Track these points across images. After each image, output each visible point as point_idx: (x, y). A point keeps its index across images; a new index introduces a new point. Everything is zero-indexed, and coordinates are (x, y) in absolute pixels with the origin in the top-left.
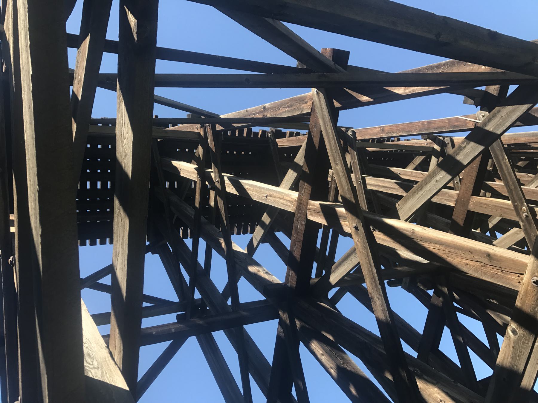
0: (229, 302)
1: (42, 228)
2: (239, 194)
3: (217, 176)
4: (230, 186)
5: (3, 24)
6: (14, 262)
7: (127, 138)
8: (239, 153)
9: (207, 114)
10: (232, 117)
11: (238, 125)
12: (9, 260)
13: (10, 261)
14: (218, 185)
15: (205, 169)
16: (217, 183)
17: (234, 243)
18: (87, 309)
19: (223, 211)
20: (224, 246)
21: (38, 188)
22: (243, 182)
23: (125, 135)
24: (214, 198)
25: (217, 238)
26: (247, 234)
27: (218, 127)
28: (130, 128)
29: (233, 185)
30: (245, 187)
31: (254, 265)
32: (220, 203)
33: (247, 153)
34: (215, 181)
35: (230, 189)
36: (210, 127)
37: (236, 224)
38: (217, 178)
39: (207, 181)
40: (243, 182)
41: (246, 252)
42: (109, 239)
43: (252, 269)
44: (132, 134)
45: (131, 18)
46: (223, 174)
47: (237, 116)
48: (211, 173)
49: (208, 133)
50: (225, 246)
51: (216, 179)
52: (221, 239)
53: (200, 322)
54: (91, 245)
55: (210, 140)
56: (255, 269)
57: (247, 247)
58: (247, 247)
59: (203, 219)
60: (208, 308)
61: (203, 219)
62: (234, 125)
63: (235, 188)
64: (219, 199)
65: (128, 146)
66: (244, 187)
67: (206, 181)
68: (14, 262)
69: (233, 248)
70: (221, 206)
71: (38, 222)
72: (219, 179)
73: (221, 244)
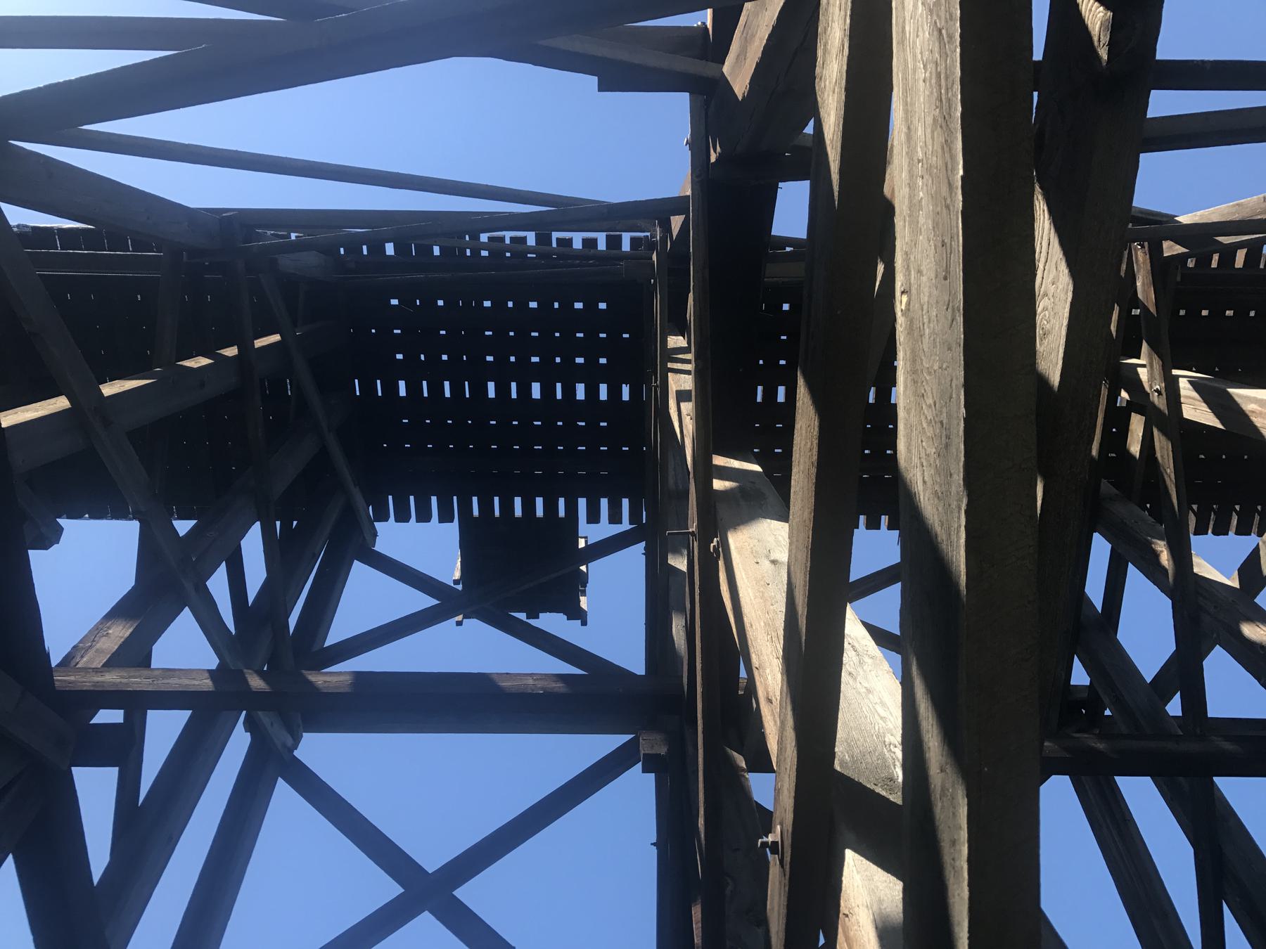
0: (1174, 707)
1: (969, 496)
2: (1223, 424)
3: (1157, 376)
4: (1197, 403)
5: (723, 63)
6: (720, 549)
7: (1050, 295)
8: (1217, 313)
9: (1140, 215)
10: (1215, 219)
11: (1236, 239)
12: (712, 545)
13: (714, 546)
14: (1160, 402)
15: (1122, 358)
16: (1156, 394)
17: (1197, 555)
18: (891, 670)
19: (1168, 471)
20: (1168, 560)
21: (964, 412)
22: (1239, 393)
23: (1046, 287)
24: (1141, 434)
25: (1145, 539)
26: (1250, 535)
27: (1171, 247)
28: (1066, 271)
29: (1205, 402)
30: (1244, 409)
31: (1259, 621)
32: (1162, 448)
33: (1241, 314)
34: (1151, 389)
35: (1196, 411)
36: (1147, 248)
37: (1237, 507)
38: (1157, 382)
39: (1126, 391)
40: (1239, 393)
41: (1235, 583)
42: (865, 516)
43: (1251, 631)
44: (1071, 288)
45: (1091, 10)
46: (1175, 372)
47: (1234, 214)
48: (1139, 370)
49: (1137, 265)
50: (1171, 562)
51: (1153, 384)
52: (1159, 542)
53: (1099, 745)
54: (868, 527)
55: (1143, 284)
56: (1262, 632)
57: (1239, 570)
58: (1240, 570)
59: (1106, 487)
60: (1108, 712)
61: (1106, 487)
62: (1220, 239)
63: (1210, 409)
64: (1160, 438)
65: (1052, 313)
66: (1241, 409)
67: (1122, 390)
68: (720, 549)
69: (1195, 570)
70: (1166, 456)
71: (958, 477)
72: (1163, 385)
73: (1156, 556)
